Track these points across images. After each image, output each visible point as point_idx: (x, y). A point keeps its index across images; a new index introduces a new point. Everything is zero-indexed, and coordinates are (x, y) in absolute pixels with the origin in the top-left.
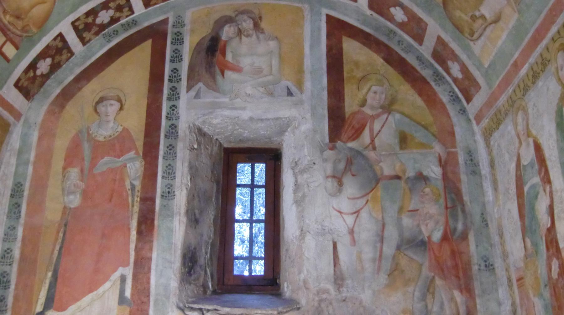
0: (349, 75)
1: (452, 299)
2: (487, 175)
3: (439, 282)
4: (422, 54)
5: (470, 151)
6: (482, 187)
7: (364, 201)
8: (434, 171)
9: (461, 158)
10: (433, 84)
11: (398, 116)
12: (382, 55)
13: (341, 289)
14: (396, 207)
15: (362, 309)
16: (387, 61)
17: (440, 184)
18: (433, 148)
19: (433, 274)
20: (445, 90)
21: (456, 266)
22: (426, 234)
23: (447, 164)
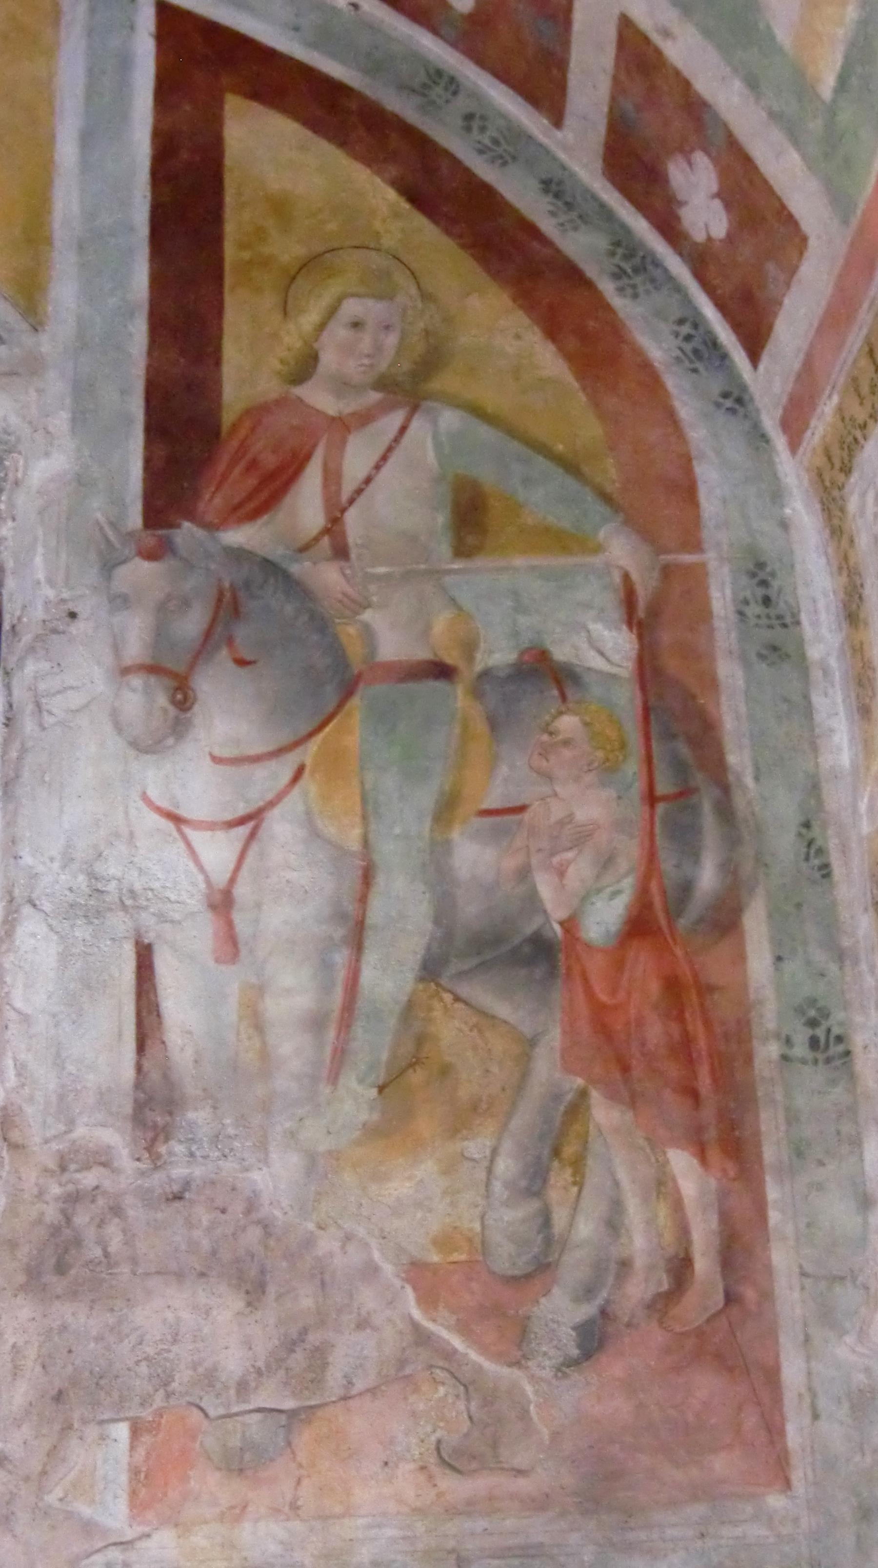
0: (246, 255)
1: (662, 1185)
2: (833, 662)
3: (604, 1113)
4: (564, 168)
5: (761, 565)
6: (808, 711)
7: (284, 770)
8: (603, 647)
9: (721, 597)
10: (607, 287)
11: (450, 419)
12: (393, 171)
13: (163, 1149)
14: (426, 798)
15: (254, 1234)
16: (417, 198)
17: (626, 699)
18: (598, 549)
19: (580, 1082)
20: (659, 314)
21: (683, 1049)
22: (557, 912)
23: (658, 616)
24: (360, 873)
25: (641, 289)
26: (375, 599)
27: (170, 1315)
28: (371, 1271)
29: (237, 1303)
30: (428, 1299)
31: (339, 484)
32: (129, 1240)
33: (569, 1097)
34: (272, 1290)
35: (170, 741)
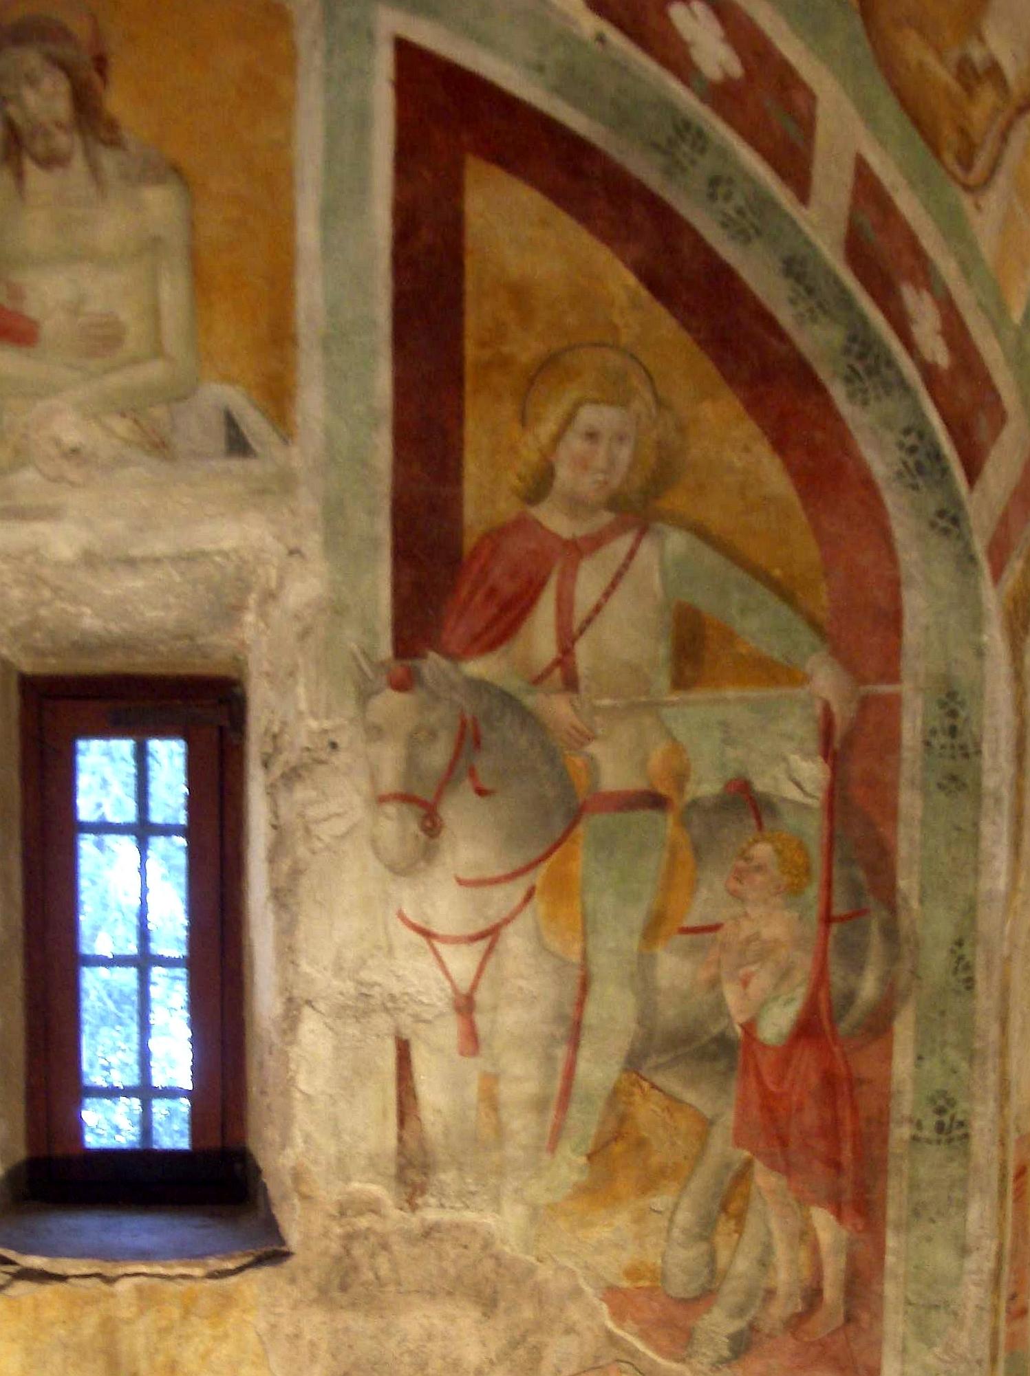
0: (487, 354)
1: (806, 1236)
3: (764, 1179)
6: (976, 838)
7: (516, 891)
10: (838, 392)
11: (677, 541)
13: (419, 1201)
14: (637, 916)
15: (489, 1265)
19: (746, 1154)
20: (887, 423)
21: (831, 1131)
23: (855, 751)
24: (578, 981)
25: (872, 394)
26: (600, 731)
27: (425, 1322)
28: (577, 1293)
29: (475, 1313)
30: (619, 1315)
31: (571, 611)
32: (395, 1267)
33: (737, 1166)
34: (502, 1305)
35: (422, 864)
